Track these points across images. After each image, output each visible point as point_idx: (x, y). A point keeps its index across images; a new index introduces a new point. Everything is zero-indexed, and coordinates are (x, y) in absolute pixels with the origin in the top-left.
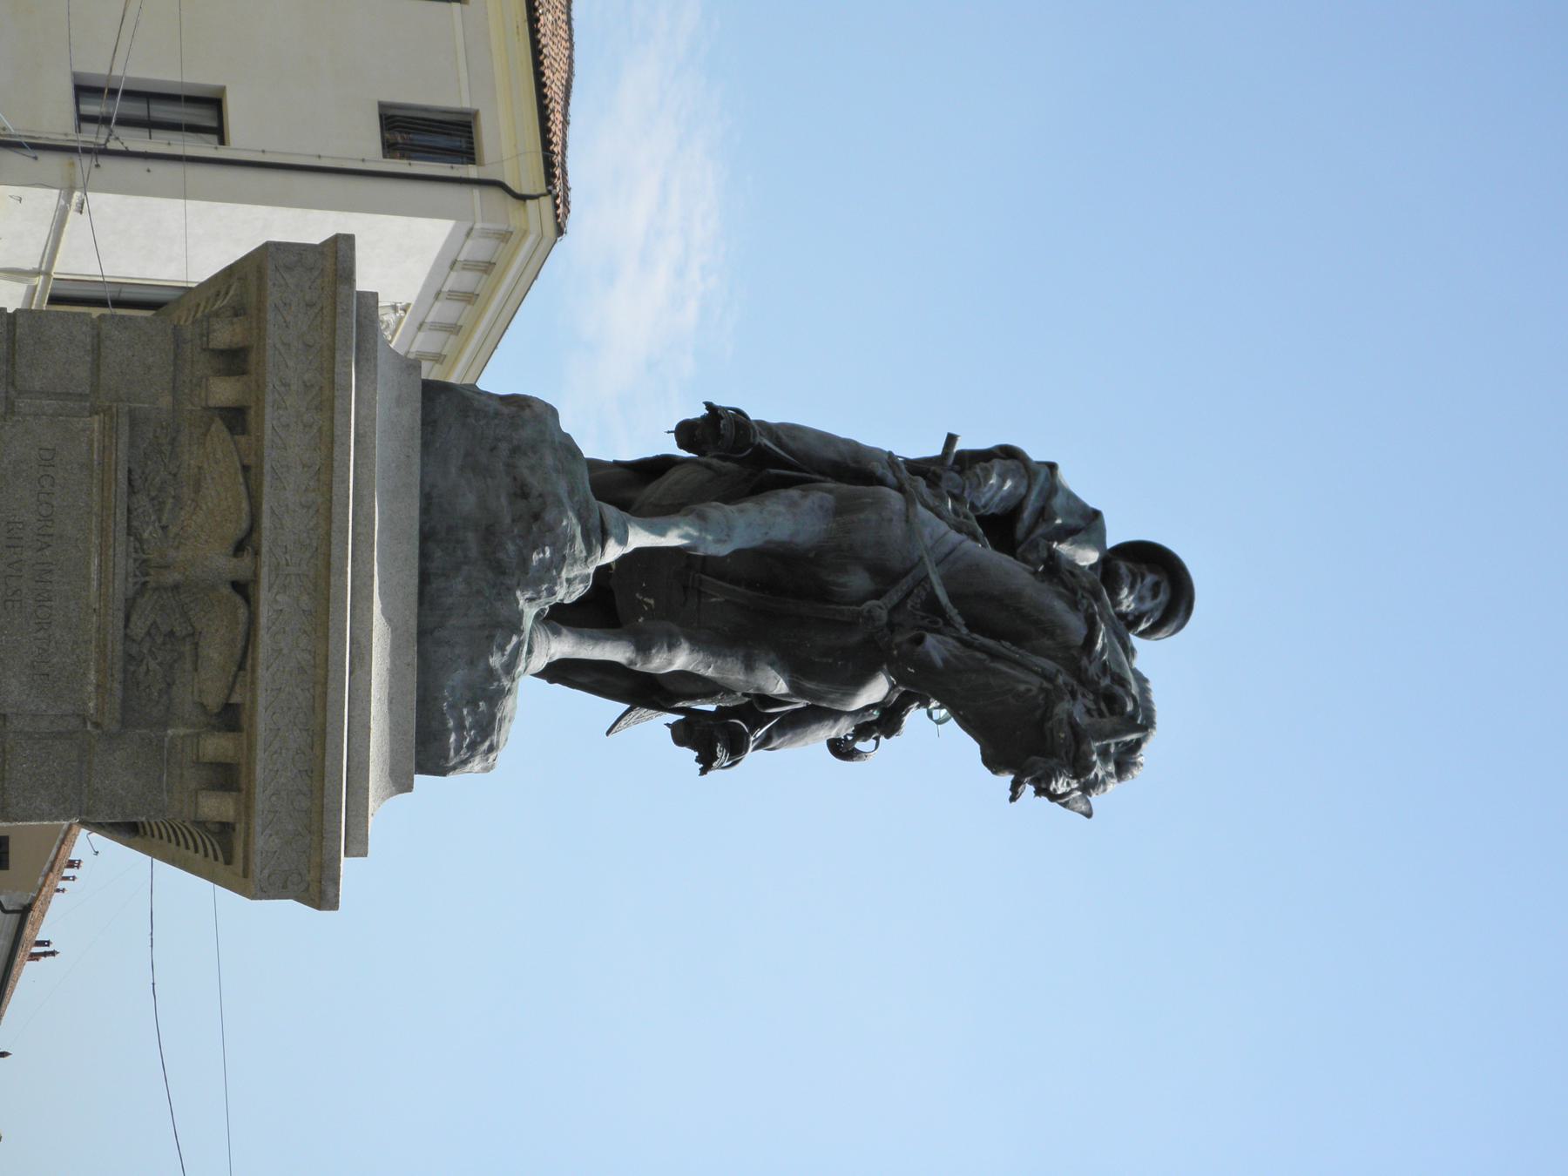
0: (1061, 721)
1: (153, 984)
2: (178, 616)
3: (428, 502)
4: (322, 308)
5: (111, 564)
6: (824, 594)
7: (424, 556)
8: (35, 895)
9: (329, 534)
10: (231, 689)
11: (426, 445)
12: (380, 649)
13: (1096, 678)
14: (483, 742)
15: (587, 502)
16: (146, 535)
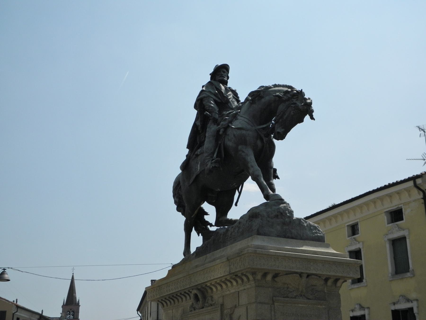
1: (28, 273)
3: (278, 236)
5: (302, 302)
7: (288, 237)
8: (14, 305)
11: (269, 236)
13: (288, 97)
16: (295, 295)
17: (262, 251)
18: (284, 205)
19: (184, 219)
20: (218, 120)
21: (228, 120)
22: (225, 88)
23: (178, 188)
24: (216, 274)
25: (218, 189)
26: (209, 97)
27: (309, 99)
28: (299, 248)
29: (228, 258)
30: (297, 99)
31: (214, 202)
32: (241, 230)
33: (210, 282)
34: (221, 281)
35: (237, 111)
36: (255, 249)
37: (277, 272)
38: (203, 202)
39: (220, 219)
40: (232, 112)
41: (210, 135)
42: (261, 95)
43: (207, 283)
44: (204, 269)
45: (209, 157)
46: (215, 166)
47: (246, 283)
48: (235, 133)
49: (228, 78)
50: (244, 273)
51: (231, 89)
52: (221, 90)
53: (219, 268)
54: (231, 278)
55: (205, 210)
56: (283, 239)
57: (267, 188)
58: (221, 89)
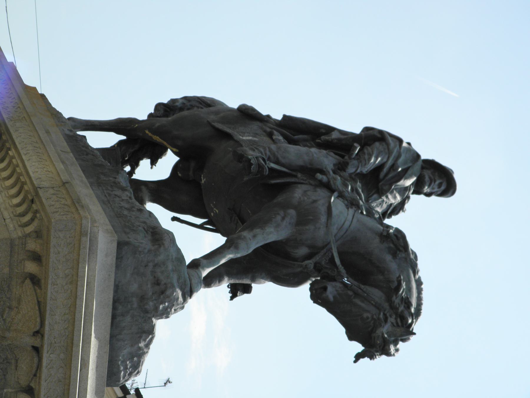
0: (379, 336)
1: (6, 7)
2: (9, 352)
3: (117, 288)
4: (74, 245)
6: (288, 256)
7: (114, 308)
9: (73, 331)
10: (30, 382)
12: (93, 351)
13: (398, 306)
14: (135, 371)
15: (185, 282)
17: (85, 248)
18: (181, 299)
19: (143, 116)
20: (344, 172)
21: (345, 190)
22: (407, 187)
23: (202, 105)
24: (34, 164)
25: (205, 180)
26: (390, 153)
27: (397, 350)
28: (94, 330)
29: (67, 183)
30: (395, 324)
31: (178, 174)
32: (126, 212)
33: (16, 156)
34: (21, 174)
35: (363, 207)
36: (89, 232)
37: (43, 281)
38: (177, 151)
39: (143, 188)
40: (361, 199)
41: (313, 155)
42: (398, 252)
43: (13, 150)
44: (42, 142)
45: (268, 153)
46: (252, 164)
47: (17, 222)
48: (321, 202)
49: (428, 195)
50: (38, 215)
51: (407, 201)
52: (404, 178)
53: (47, 169)
54: (27, 192)
55: (160, 160)
56: (111, 296)
57: (213, 266)
58: (407, 178)
